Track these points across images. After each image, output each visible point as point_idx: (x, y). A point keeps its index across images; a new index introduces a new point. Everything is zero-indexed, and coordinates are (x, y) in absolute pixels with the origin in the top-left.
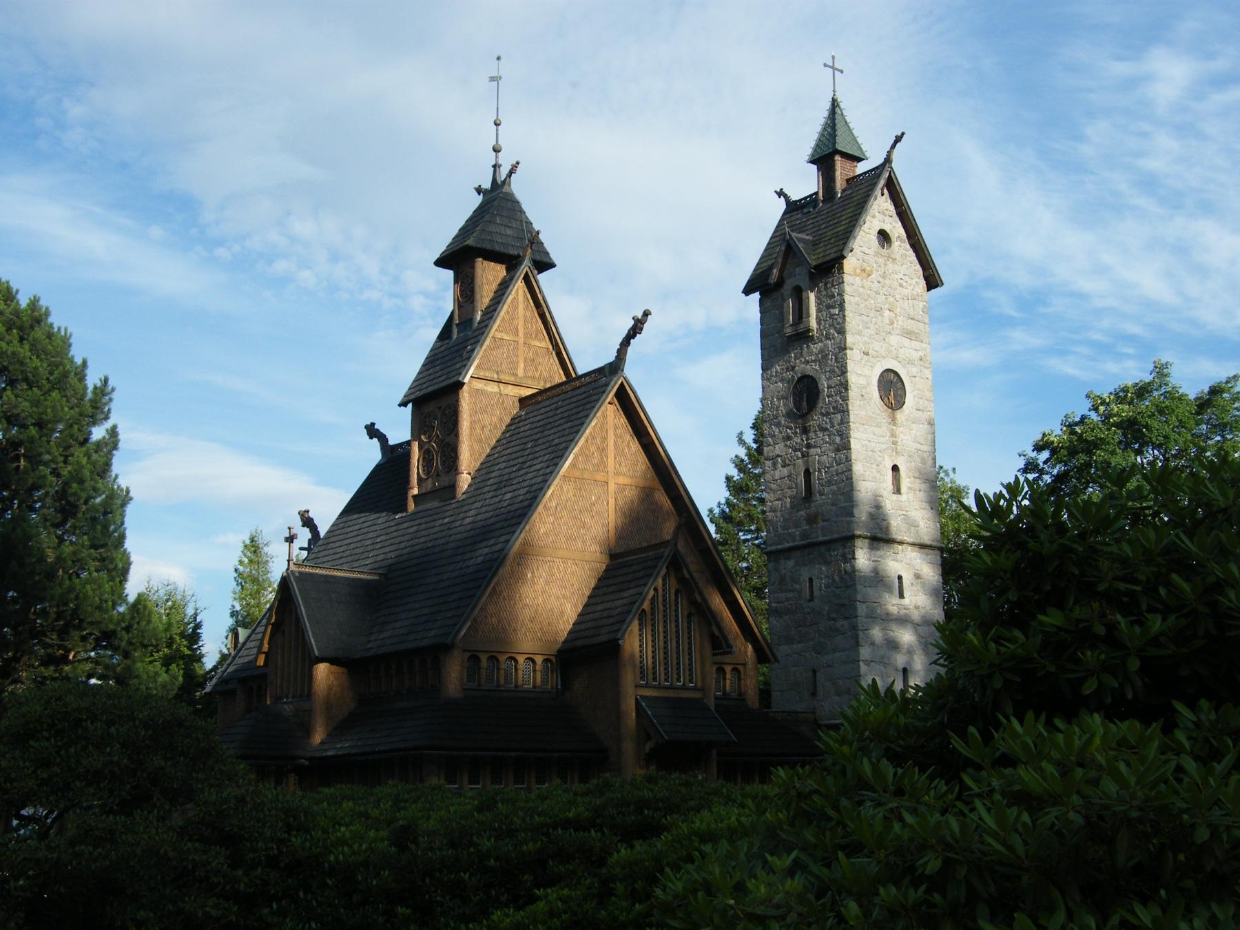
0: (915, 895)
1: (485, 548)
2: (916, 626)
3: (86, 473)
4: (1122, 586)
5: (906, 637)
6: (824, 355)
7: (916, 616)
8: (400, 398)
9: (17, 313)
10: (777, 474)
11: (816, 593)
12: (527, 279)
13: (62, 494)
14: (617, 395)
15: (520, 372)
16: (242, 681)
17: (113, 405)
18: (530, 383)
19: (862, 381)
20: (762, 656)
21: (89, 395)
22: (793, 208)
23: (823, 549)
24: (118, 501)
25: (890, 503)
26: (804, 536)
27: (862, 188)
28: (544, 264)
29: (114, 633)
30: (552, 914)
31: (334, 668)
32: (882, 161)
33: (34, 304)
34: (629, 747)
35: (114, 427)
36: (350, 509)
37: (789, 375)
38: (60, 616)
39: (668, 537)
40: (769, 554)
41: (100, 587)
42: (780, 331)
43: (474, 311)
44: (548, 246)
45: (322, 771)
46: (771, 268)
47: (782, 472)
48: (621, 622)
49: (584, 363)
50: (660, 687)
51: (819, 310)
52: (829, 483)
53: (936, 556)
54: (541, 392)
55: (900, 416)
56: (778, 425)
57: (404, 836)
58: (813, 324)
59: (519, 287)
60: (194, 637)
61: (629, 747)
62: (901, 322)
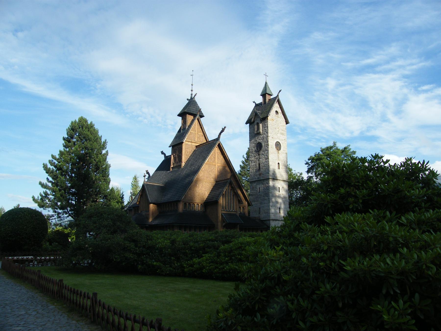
0: (320, 255)
1: (188, 179)
2: (282, 198)
3: (102, 160)
4: (357, 184)
5: (280, 200)
6: (263, 137)
7: (282, 196)
8: (169, 145)
9: (87, 125)
10: (252, 164)
11: (261, 191)
12: (198, 119)
13: (96, 165)
14: (218, 145)
15: (196, 140)
16: (134, 208)
17: (107, 146)
19: (272, 144)
20: (249, 205)
21: (102, 143)
22: (257, 105)
24: (108, 167)
25: (277, 171)
26: (258, 178)
27: (272, 102)
28: (202, 116)
29: (107, 196)
30: (207, 260)
31: (154, 205)
33: (91, 123)
34: (220, 224)
36: (157, 170)
37: (255, 142)
38: (96, 191)
39: (228, 178)
40: (250, 182)
41: (104, 185)
42: (254, 132)
43: (186, 126)
44: (203, 112)
45: (152, 227)
46: (252, 118)
47: (253, 164)
48: (218, 197)
49: (211, 138)
50: (227, 211)
51: (262, 128)
52: (264, 166)
53: (287, 183)
54: (201, 145)
55: (280, 151)
56: (253, 153)
57: (173, 242)
58: (261, 131)
59: (196, 121)
60: (122, 198)
61: (220, 224)
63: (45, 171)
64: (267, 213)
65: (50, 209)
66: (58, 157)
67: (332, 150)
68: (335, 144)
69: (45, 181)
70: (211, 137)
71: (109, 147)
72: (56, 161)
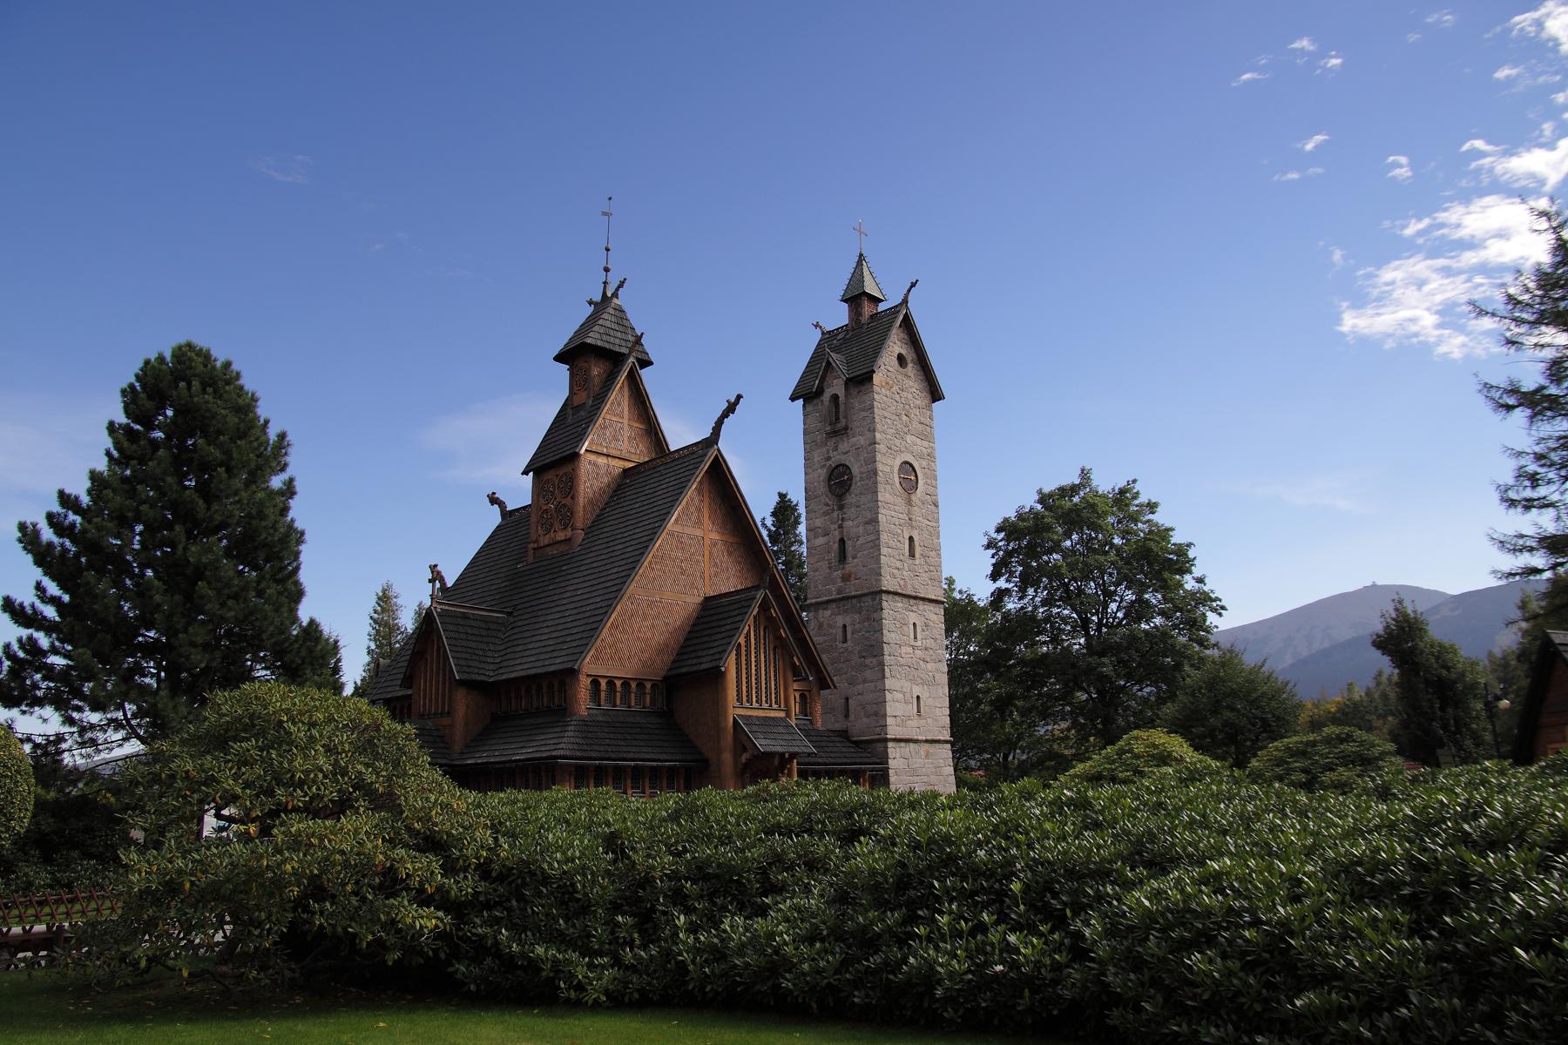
18: (633, 458)
19: (887, 469)
24: (293, 538)
34: (727, 757)
35: (291, 480)
62: (915, 424)
63: (30, 558)
64: (876, 714)
65: (48, 711)
66: (85, 500)
67: (1076, 499)
68: (1085, 474)
69: (26, 596)
70: (680, 433)
71: (299, 465)
72: (78, 519)
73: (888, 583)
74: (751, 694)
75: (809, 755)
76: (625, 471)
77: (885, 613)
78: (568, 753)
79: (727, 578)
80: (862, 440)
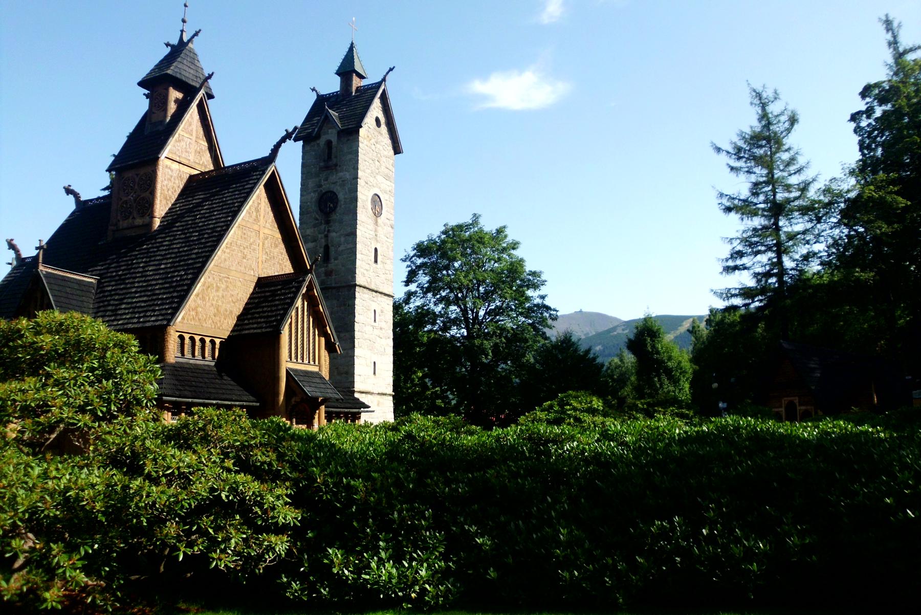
19: (364, 198)
23: (334, 291)
32: (380, 80)
55: (380, 220)
62: (383, 169)
68: (476, 217)
70: (234, 155)
73: (357, 283)
74: (299, 351)
75: (337, 400)
76: (191, 177)
77: (357, 302)
78: (170, 392)
79: (282, 266)
80: (347, 176)
